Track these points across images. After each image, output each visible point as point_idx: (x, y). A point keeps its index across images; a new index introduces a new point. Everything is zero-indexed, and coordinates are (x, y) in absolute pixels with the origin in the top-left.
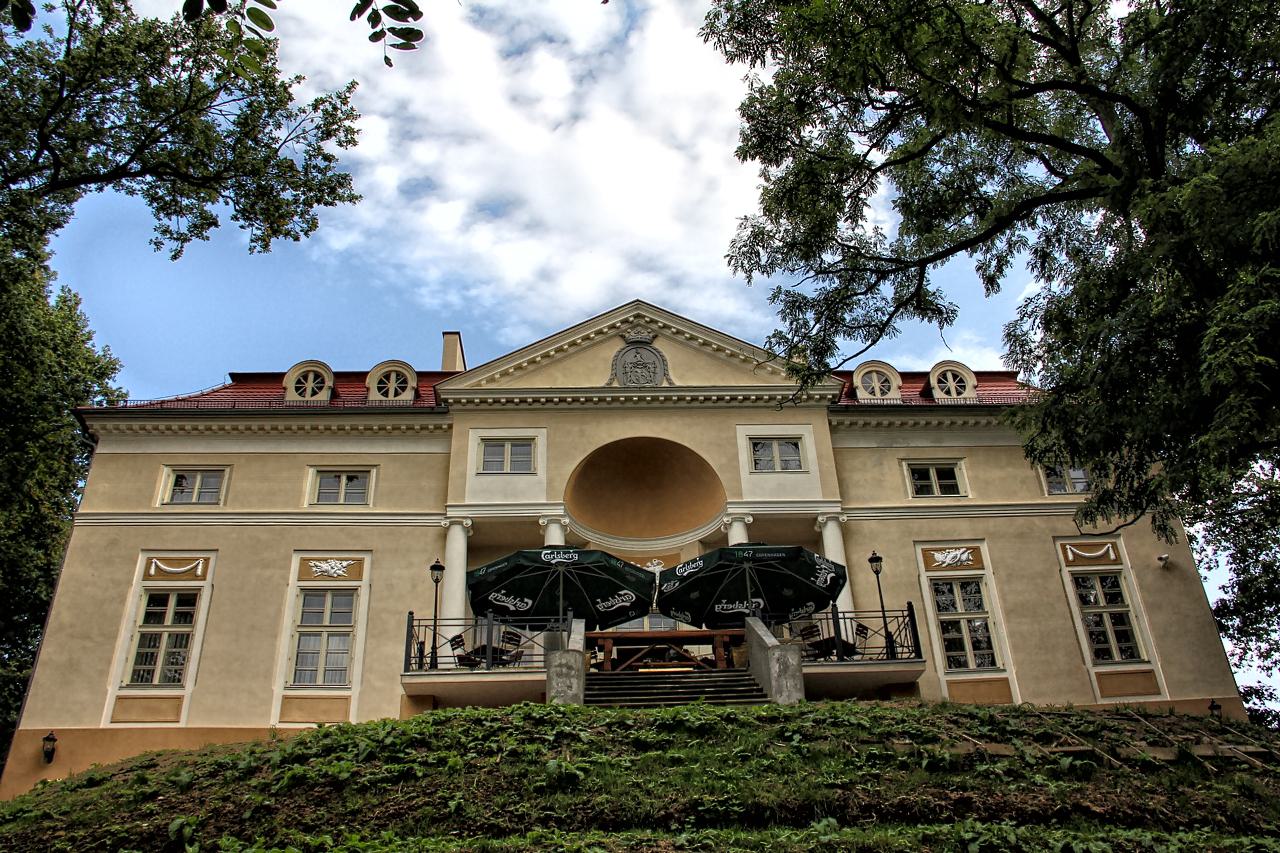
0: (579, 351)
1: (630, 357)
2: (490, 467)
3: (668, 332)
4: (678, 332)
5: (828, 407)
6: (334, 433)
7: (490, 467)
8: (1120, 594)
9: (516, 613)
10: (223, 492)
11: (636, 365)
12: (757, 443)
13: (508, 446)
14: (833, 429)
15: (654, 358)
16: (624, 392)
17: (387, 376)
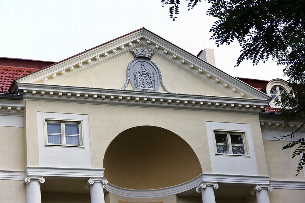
0: (113, 57)
1: (138, 67)
2: (54, 141)
3: (161, 52)
4: (168, 53)
5: (260, 113)
7: (54, 141)
11: (142, 74)
12: (53, 124)
13: (63, 126)
14: (262, 127)
15: (153, 70)
16: (139, 94)
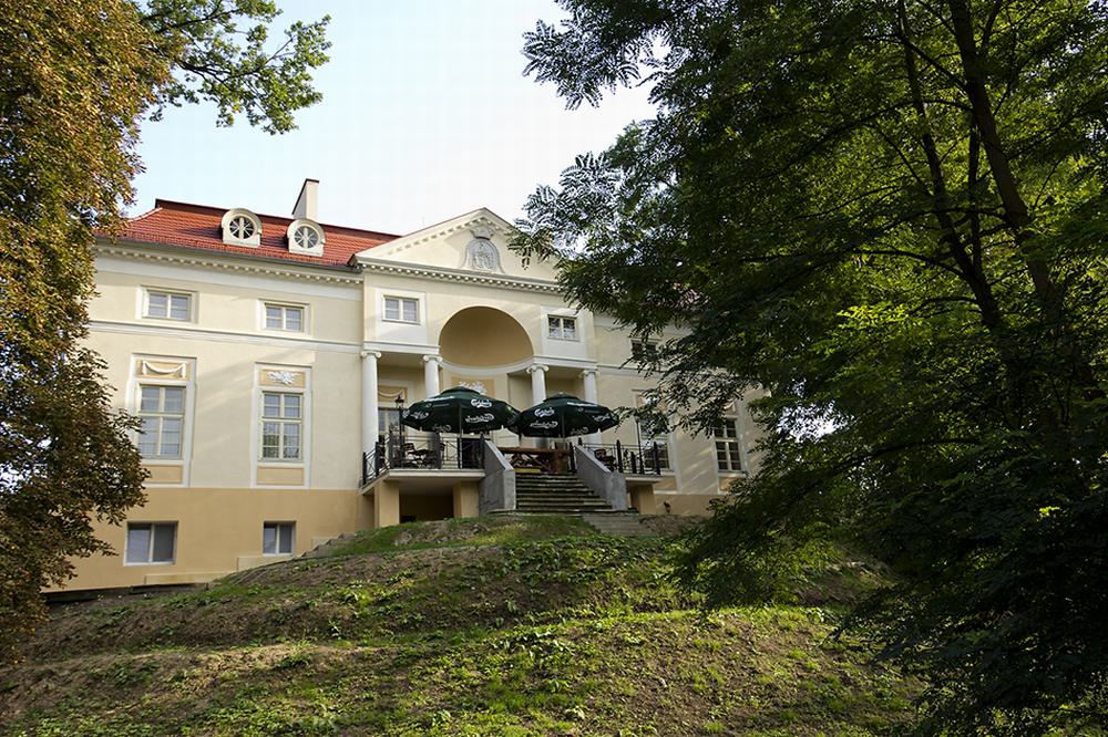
3: (500, 233)
6: (277, 276)
8: (734, 432)
9: (550, 429)
10: (193, 312)
17: (237, 220)
